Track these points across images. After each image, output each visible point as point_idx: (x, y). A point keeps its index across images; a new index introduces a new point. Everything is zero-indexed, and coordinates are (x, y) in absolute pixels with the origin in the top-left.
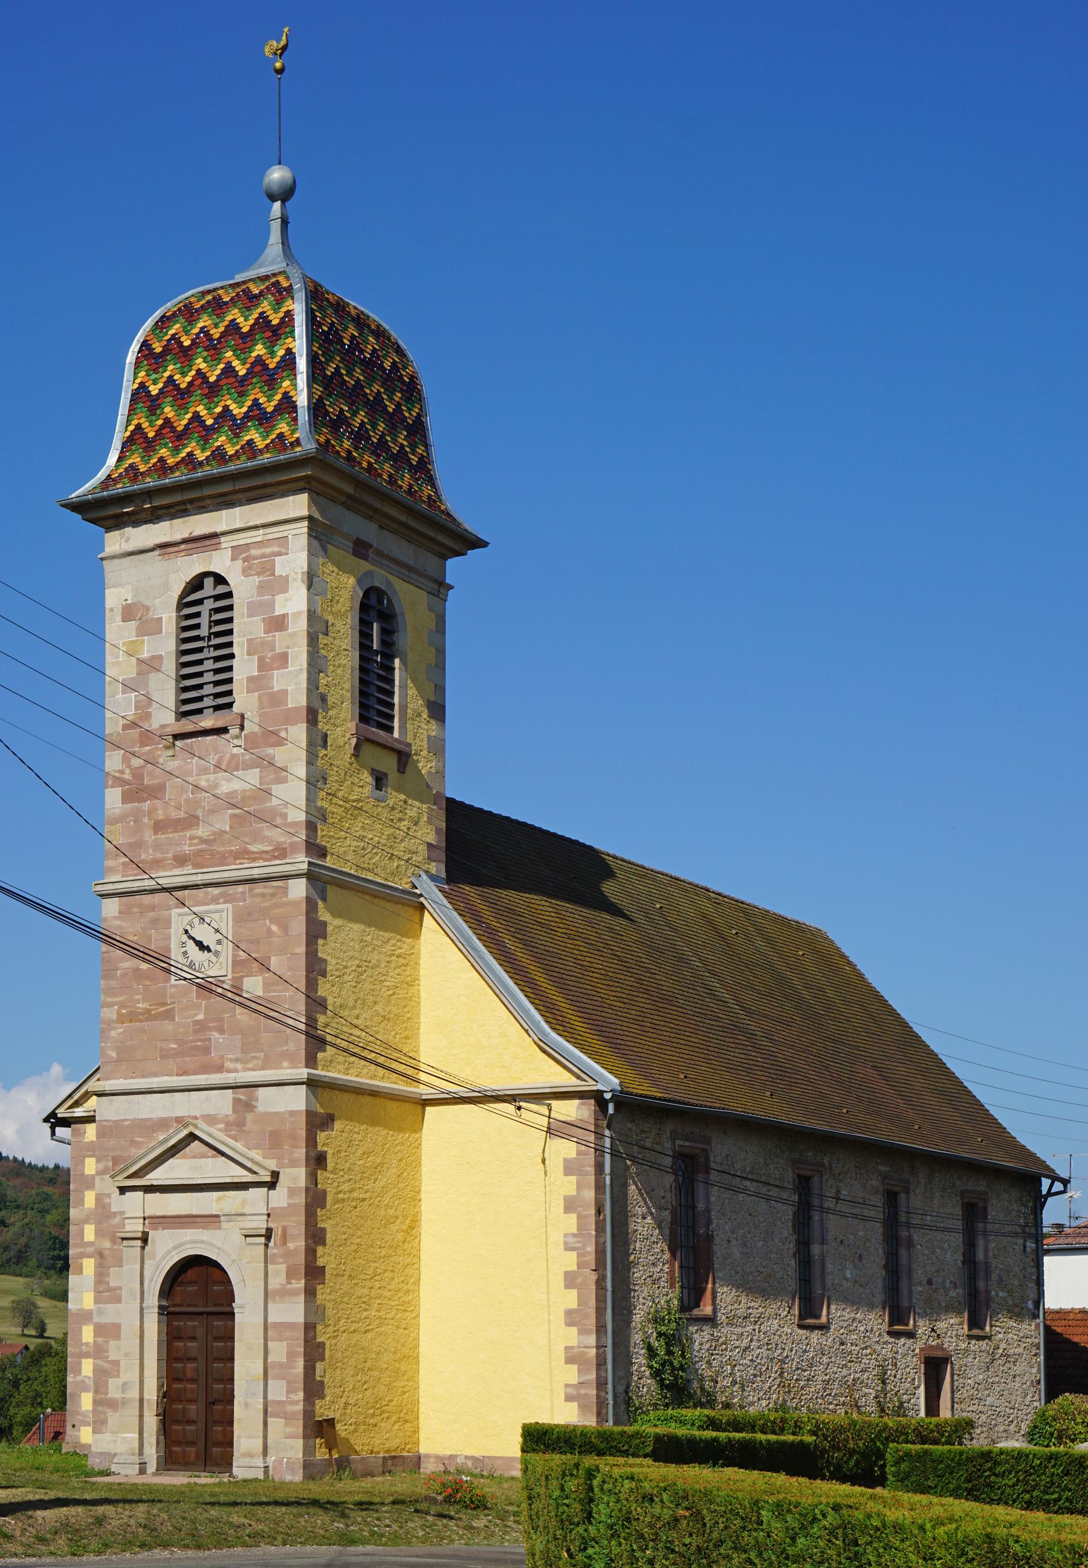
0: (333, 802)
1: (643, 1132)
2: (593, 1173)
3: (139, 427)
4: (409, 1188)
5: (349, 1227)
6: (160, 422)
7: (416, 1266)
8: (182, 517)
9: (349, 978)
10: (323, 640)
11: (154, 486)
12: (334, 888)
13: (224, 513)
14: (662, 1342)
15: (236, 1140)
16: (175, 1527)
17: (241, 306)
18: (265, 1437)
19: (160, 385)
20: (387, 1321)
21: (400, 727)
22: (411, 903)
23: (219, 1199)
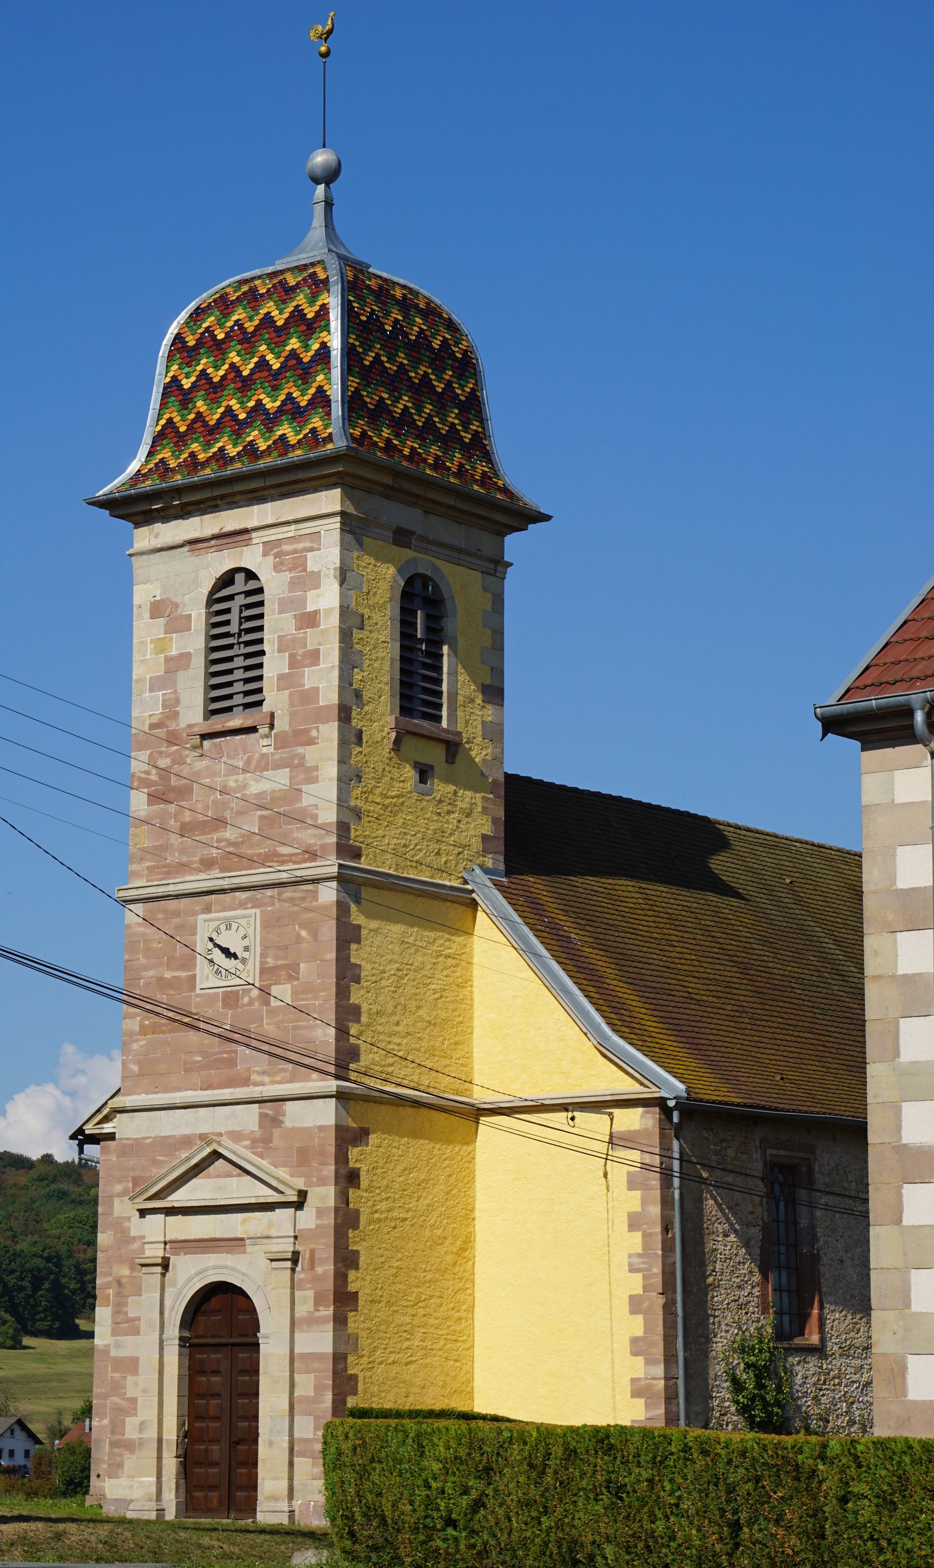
0: (370, 799)
1: (723, 1140)
2: (659, 1187)
3: (170, 421)
4: (460, 1206)
5: (386, 1249)
6: (192, 416)
7: (468, 1292)
9: (387, 983)
10: (357, 634)
12: (370, 890)
14: (751, 1374)
15: (262, 1158)
16: (137, 1545)
18: (291, 1479)
19: (193, 379)
20: (433, 1352)
21: (449, 716)
22: (461, 900)
23: (244, 1221)
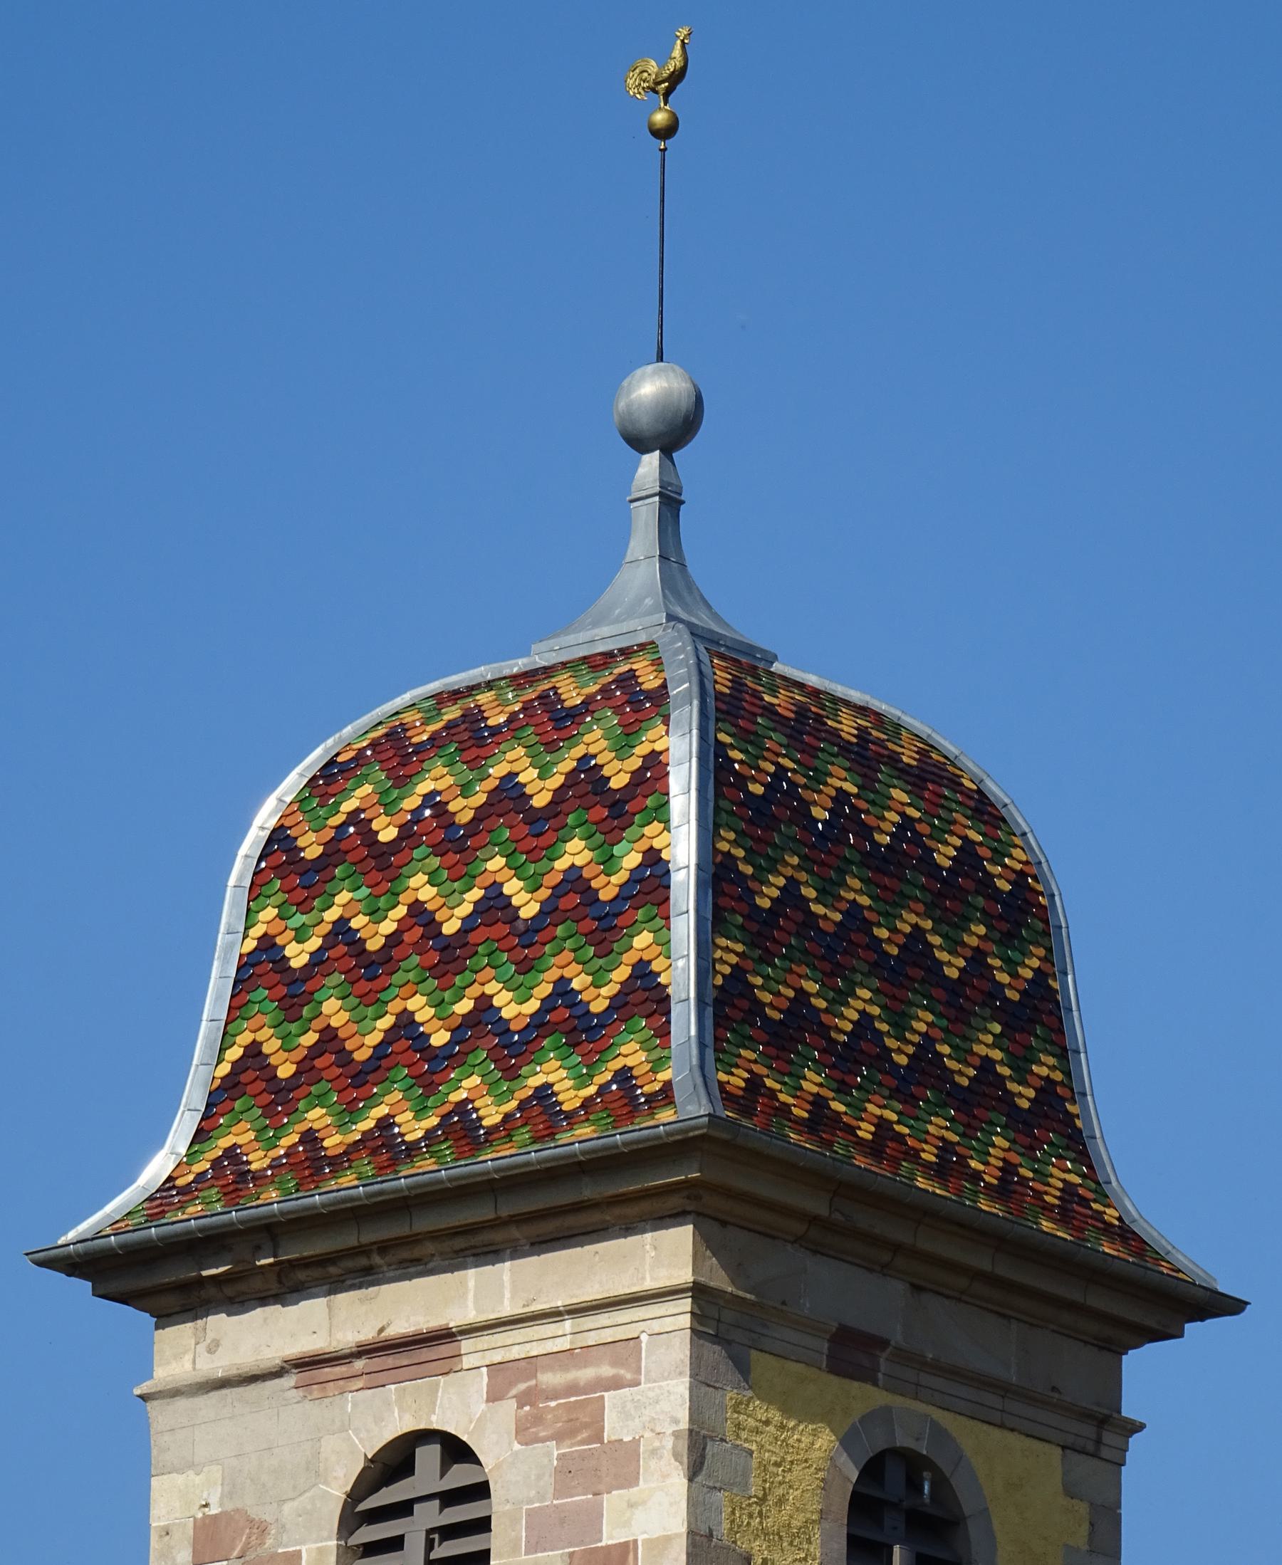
6: (310, 1038)
8: (360, 1286)
11: (282, 1213)
13: (472, 1276)
17: (534, 739)
19: (315, 943)
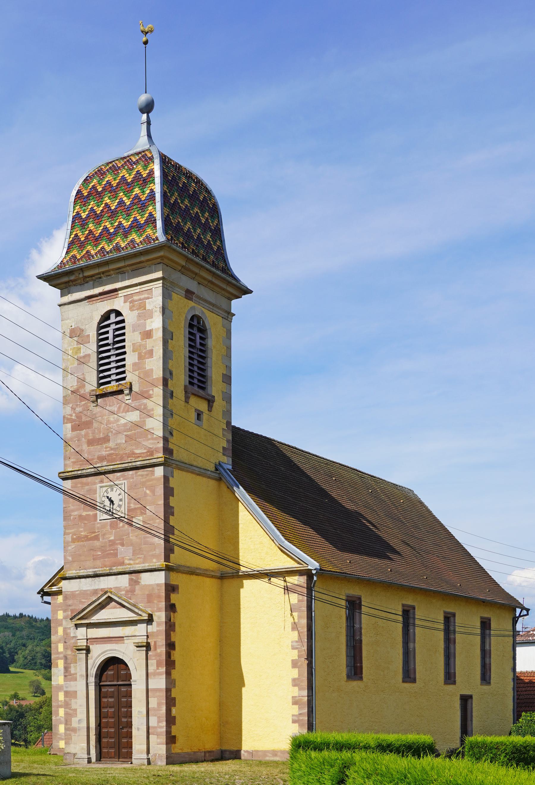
2: (306, 611)
3: (76, 235)
6: (87, 232)
